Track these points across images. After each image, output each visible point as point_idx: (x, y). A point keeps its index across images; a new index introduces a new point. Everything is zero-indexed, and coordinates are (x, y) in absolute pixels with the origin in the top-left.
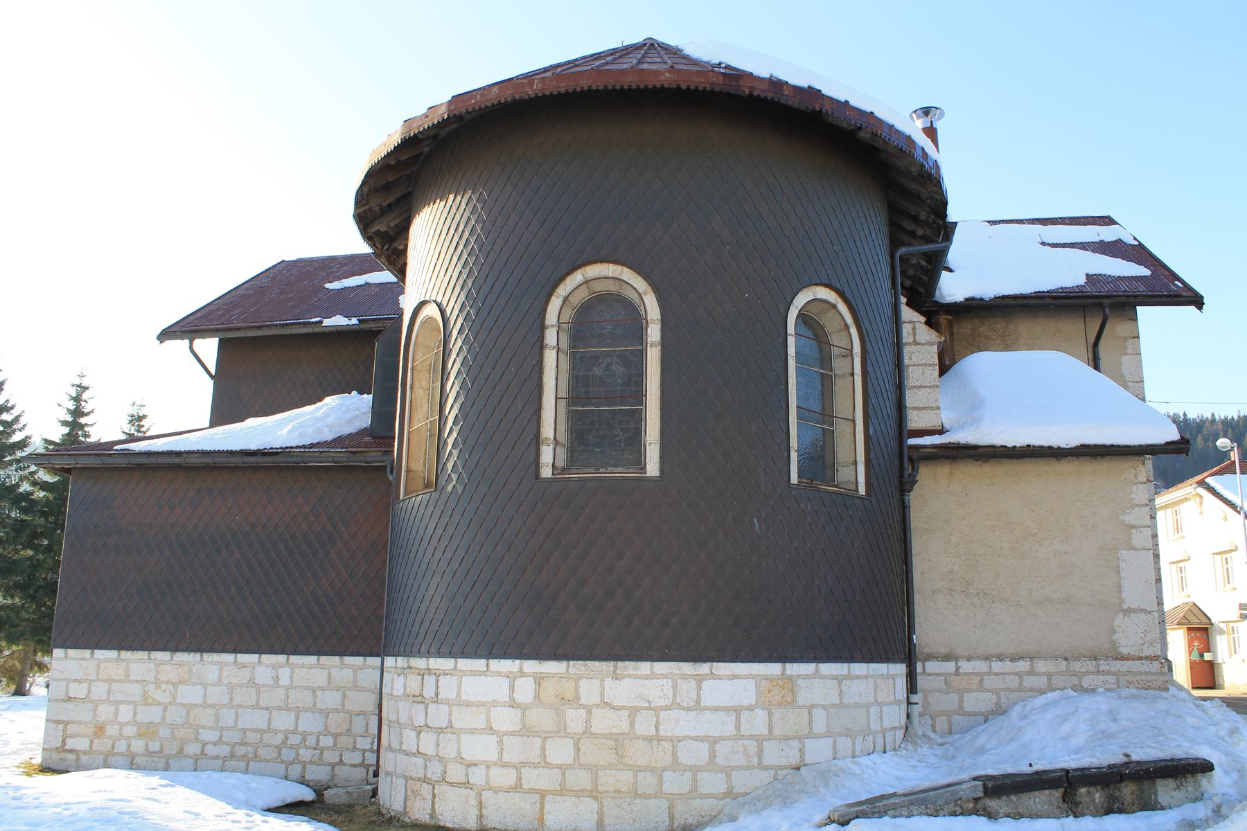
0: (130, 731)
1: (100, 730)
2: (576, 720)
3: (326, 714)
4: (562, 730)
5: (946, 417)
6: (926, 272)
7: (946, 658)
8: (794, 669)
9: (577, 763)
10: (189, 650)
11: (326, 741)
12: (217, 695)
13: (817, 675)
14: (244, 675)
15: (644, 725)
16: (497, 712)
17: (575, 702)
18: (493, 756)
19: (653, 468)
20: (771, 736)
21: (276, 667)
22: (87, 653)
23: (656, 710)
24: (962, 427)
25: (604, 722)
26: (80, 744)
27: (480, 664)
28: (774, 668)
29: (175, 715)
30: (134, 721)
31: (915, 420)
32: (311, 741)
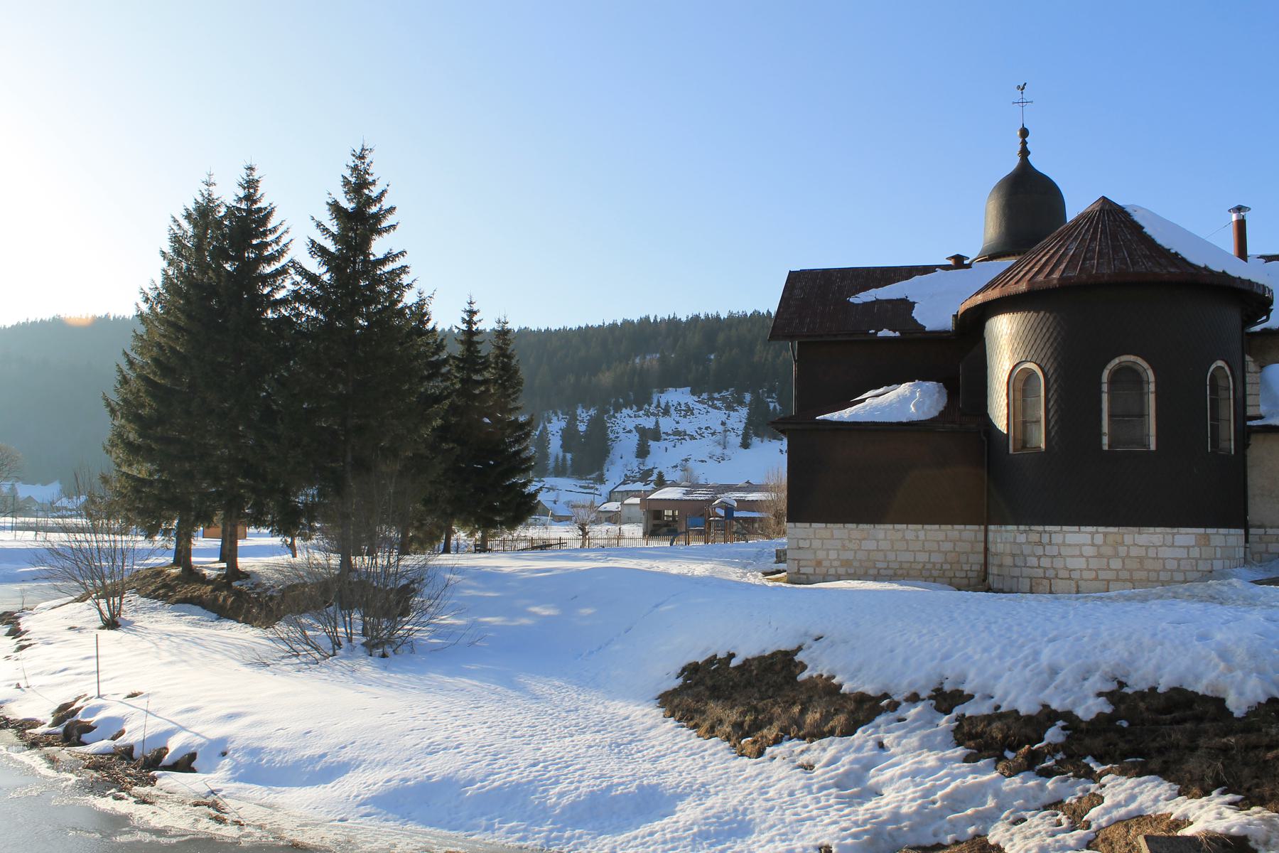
0: (836, 563)
1: (819, 563)
2: (1122, 551)
3: (946, 553)
4: (1116, 555)
5: (1263, 410)
7: (1259, 527)
8: (1209, 531)
9: (1124, 568)
10: (867, 523)
11: (946, 566)
12: (884, 545)
13: (1217, 534)
14: (900, 535)
15: (1152, 553)
16: (1084, 548)
17: (1122, 544)
18: (1084, 566)
19: (1153, 447)
20: (1200, 558)
21: (916, 531)
22: (807, 525)
23: (1156, 547)
24: (1272, 416)
25: (1134, 552)
26: (809, 570)
27: (1076, 528)
28: (1201, 530)
29: (861, 555)
30: (838, 559)
31: (1250, 411)
32: (938, 566)
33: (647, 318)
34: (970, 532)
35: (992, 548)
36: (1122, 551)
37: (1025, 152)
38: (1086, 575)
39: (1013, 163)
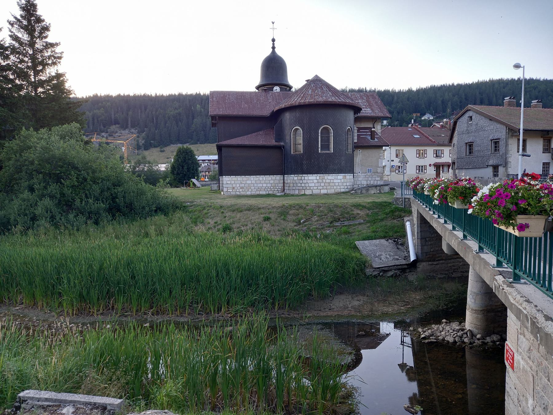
1: (234, 188)
2: (324, 181)
4: (323, 182)
6: (437, 236)
12: (254, 182)
25: (327, 181)
33: (97, 95)
34: (279, 177)
35: (286, 182)
36: (324, 181)
37: (273, 48)
38: (315, 188)
39: (269, 52)
